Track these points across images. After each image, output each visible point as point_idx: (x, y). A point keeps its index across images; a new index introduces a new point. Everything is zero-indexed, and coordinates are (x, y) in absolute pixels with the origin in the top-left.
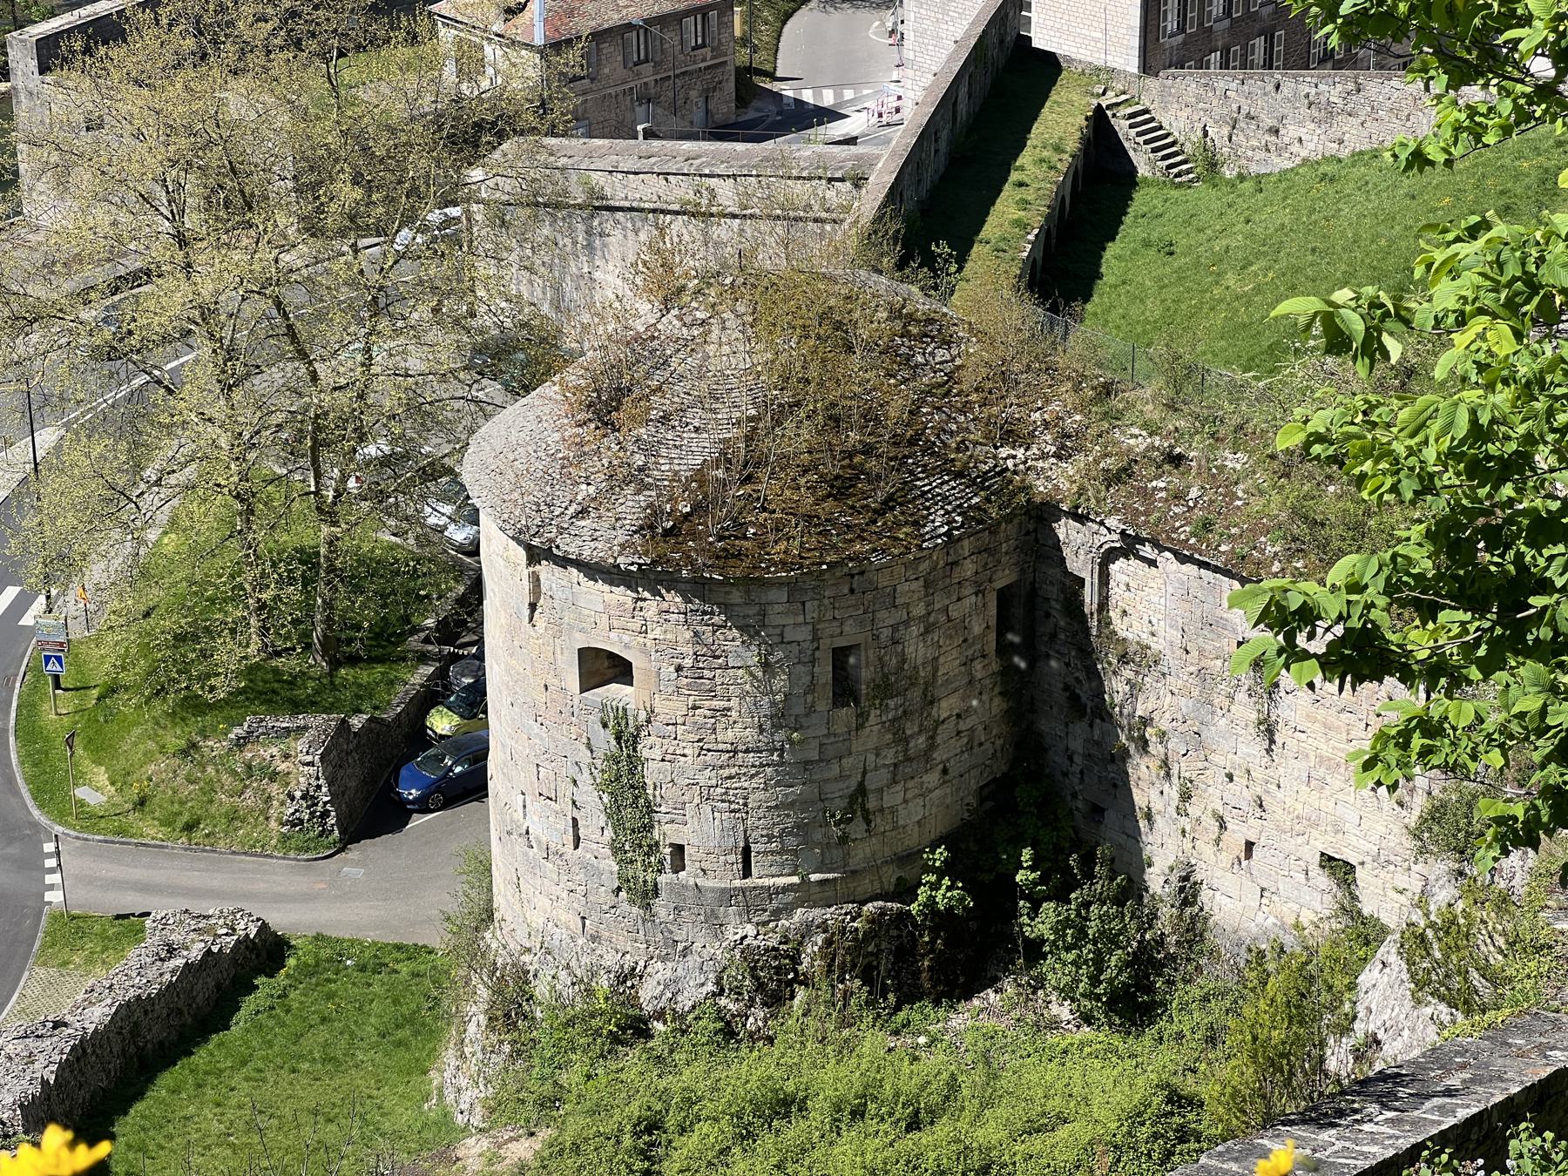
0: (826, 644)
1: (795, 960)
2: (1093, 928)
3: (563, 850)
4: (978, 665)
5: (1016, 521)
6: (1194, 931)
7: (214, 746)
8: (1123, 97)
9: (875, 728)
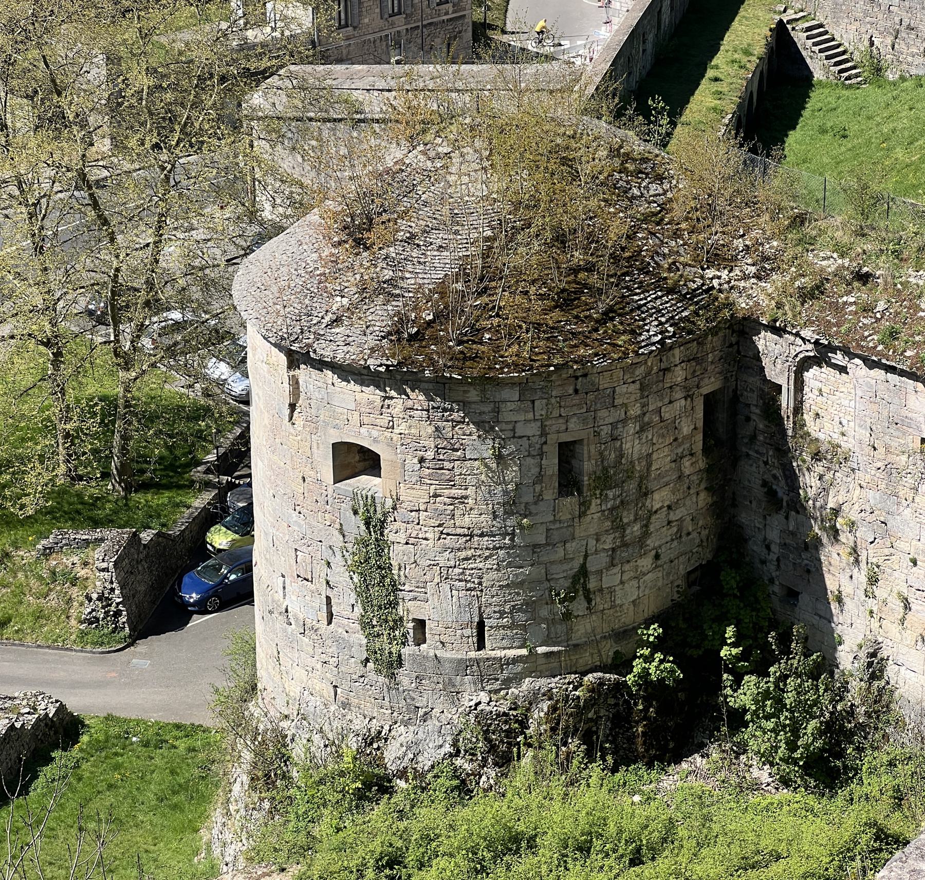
0: (553, 438)
1: (524, 725)
2: (789, 698)
3: (318, 626)
4: (686, 463)
5: (721, 334)
6: (882, 702)
7: (24, 556)
8: (801, 14)
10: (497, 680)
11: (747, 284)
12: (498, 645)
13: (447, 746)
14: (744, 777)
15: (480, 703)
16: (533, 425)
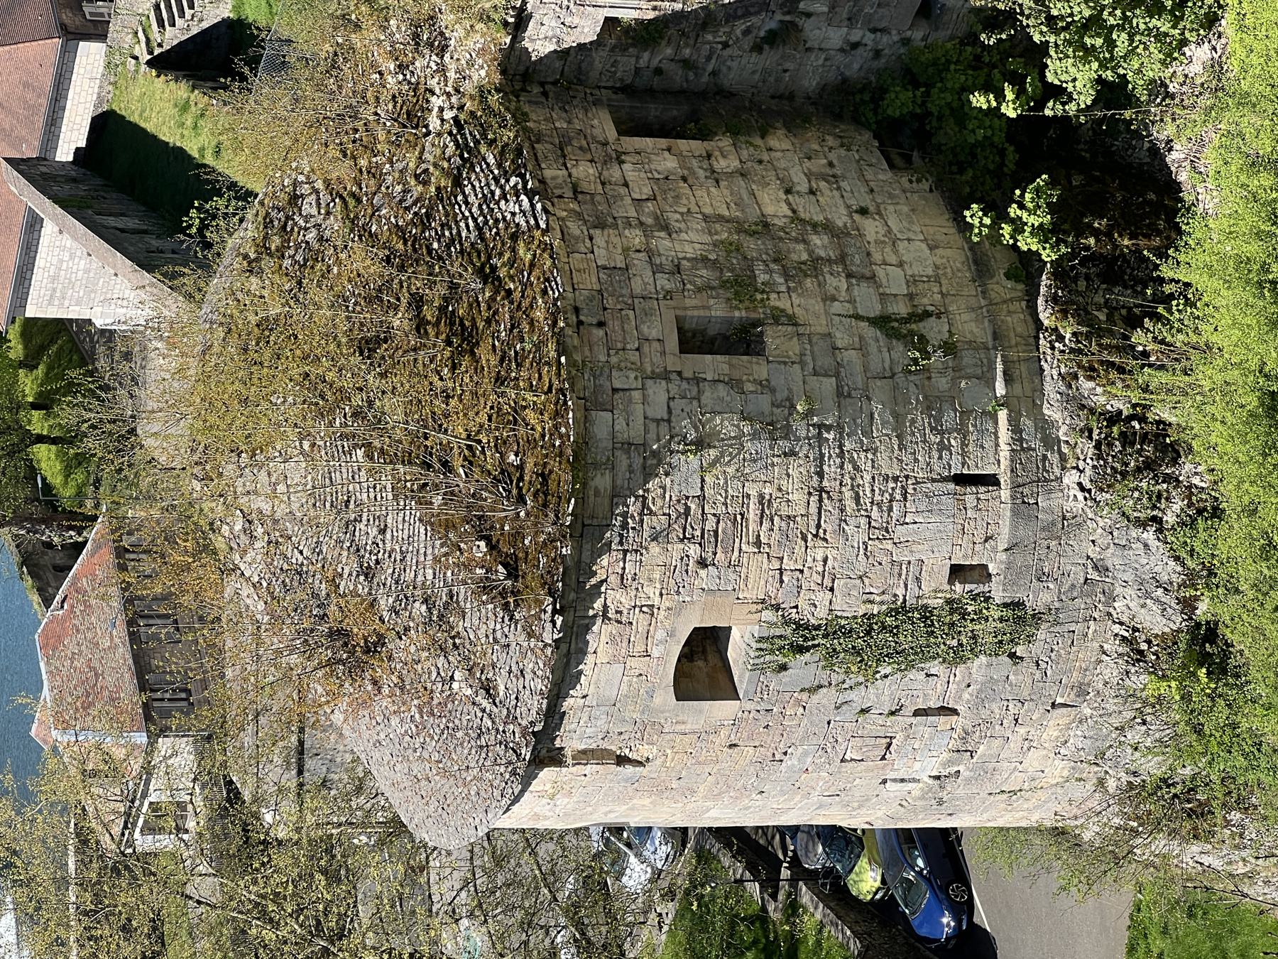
0: (674, 361)
1: (1114, 418)
4: (721, 164)
5: (526, 108)
8: (141, 34)
9: (796, 301)
10: (1045, 457)
11: (452, 67)
12: (991, 454)
13: (1145, 535)
14: (1202, 84)
15: (1080, 484)
16: (650, 392)
